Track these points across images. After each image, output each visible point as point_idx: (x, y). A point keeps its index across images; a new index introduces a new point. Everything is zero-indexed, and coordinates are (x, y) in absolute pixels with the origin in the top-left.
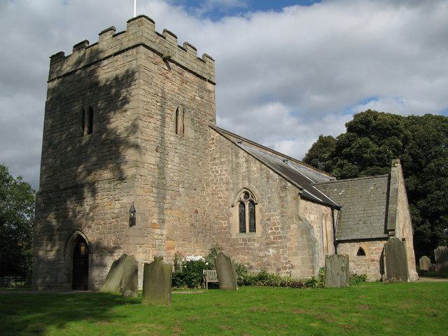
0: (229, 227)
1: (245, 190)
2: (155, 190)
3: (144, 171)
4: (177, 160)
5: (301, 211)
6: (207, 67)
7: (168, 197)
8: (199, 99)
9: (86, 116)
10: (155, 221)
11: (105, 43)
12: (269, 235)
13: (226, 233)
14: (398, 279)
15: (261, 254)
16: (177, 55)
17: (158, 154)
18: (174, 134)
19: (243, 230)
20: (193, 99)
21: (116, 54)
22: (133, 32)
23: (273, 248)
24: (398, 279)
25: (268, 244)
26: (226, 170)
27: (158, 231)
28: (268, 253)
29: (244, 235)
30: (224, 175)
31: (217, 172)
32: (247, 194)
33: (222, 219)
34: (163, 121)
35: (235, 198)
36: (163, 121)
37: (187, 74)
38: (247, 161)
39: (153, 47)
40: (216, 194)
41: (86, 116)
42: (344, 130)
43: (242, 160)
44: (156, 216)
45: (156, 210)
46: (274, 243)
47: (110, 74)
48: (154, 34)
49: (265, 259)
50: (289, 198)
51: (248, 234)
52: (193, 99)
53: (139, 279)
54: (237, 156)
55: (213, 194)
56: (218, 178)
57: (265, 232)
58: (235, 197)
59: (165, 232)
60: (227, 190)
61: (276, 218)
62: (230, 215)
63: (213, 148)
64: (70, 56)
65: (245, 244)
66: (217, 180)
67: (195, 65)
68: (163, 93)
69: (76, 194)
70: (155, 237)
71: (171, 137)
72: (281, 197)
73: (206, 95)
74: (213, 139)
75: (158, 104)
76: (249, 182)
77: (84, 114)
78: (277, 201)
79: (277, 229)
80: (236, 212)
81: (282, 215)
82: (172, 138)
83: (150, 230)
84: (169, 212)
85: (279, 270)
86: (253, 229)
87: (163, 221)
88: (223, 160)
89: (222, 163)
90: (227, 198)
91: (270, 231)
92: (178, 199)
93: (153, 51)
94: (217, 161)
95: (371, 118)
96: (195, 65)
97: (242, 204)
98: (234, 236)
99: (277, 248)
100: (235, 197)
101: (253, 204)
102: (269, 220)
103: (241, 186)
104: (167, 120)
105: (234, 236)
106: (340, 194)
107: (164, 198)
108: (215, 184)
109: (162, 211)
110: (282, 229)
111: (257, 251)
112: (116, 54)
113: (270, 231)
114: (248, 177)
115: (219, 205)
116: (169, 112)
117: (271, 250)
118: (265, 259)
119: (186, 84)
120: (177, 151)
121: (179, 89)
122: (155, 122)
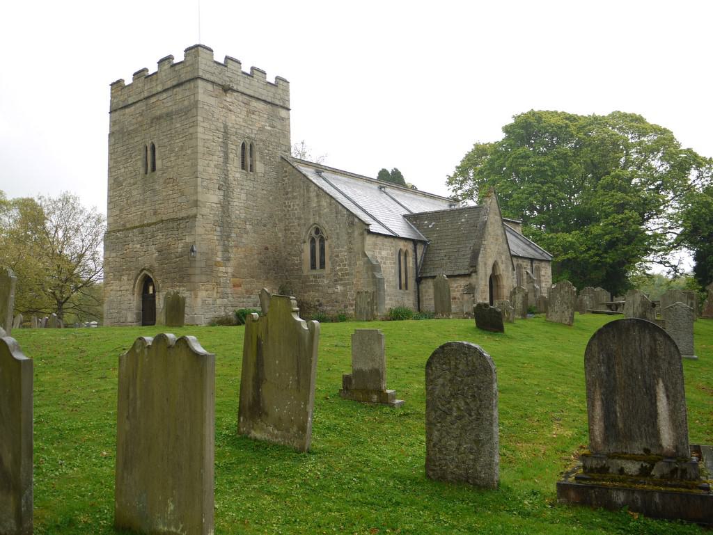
0: (301, 264)
1: (315, 225)
2: (218, 229)
3: (205, 211)
4: (243, 196)
5: (367, 247)
6: (280, 92)
7: (233, 235)
8: (269, 128)
9: (149, 152)
10: (219, 259)
11: (163, 74)
12: (338, 271)
13: (298, 269)
14: (443, 315)
15: (330, 291)
16: (242, 84)
17: (222, 193)
18: (240, 170)
19: (313, 267)
20: (262, 129)
21: (174, 87)
22: (190, 62)
23: (341, 285)
24: (443, 315)
25: (336, 281)
26: (298, 205)
27: (222, 269)
28: (336, 290)
29: (314, 272)
30: (296, 209)
31: (290, 207)
32: (317, 231)
33: (295, 256)
34: (226, 158)
35: (305, 235)
36: (226, 158)
37: (254, 104)
38: (318, 196)
39: (212, 78)
40: (289, 230)
41: (149, 152)
42: (500, 136)
43: (313, 195)
44: (220, 254)
45: (220, 248)
46: (341, 280)
47: (171, 108)
48: (212, 64)
49: (333, 296)
50: (356, 233)
51: (318, 272)
52: (262, 129)
53: (432, 296)
54: (308, 191)
55: (285, 230)
56: (291, 212)
57: (333, 269)
58: (307, 232)
59: (230, 270)
60: (299, 225)
61: (344, 254)
62: (302, 251)
63: (286, 181)
64: (156, 73)
65: (316, 281)
66: (290, 216)
67: (264, 92)
68: (226, 127)
69: (142, 233)
70: (219, 275)
71: (235, 172)
72: (348, 233)
73: (278, 124)
74: (286, 172)
75: (221, 140)
76: (320, 217)
77: (147, 151)
78: (345, 237)
79: (345, 265)
80: (307, 248)
81: (350, 251)
82: (238, 175)
83: (215, 268)
84: (235, 249)
85: (346, 307)
86: (323, 265)
87: (228, 259)
88: (295, 194)
89: (294, 198)
90: (299, 234)
91: (338, 268)
92: (245, 236)
93: (213, 83)
94: (290, 195)
95: (532, 120)
96: (264, 92)
97: (313, 241)
98: (305, 273)
99: (344, 285)
100: (307, 232)
101: (322, 240)
102: (337, 256)
103: (312, 222)
104: (231, 156)
105: (305, 273)
106: (430, 226)
107: (229, 236)
108: (288, 219)
109: (226, 249)
110: (350, 265)
111: (327, 288)
112: (174, 87)
113: (338, 268)
114: (318, 212)
115: (292, 241)
116: (234, 147)
117: (339, 287)
118: (333, 296)
119: (253, 114)
120: (243, 187)
121: (245, 121)
122: (218, 158)
